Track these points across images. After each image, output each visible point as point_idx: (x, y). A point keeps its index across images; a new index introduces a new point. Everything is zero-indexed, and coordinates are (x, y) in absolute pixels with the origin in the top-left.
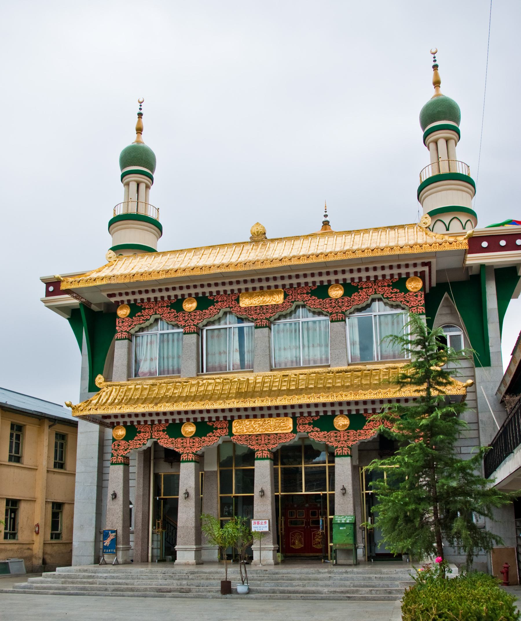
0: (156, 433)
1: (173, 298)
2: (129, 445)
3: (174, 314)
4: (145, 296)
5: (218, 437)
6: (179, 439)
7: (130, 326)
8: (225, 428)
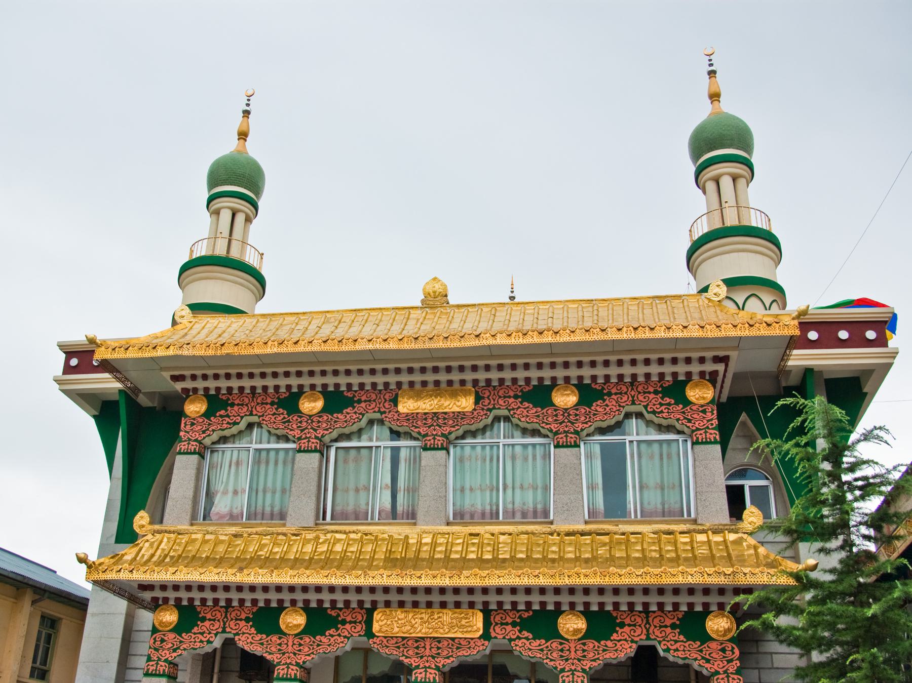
2: (181, 642)
4: (235, 384)
5: (345, 637)
6: (275, 638)
7: (204, 432)
8: (360, 622)
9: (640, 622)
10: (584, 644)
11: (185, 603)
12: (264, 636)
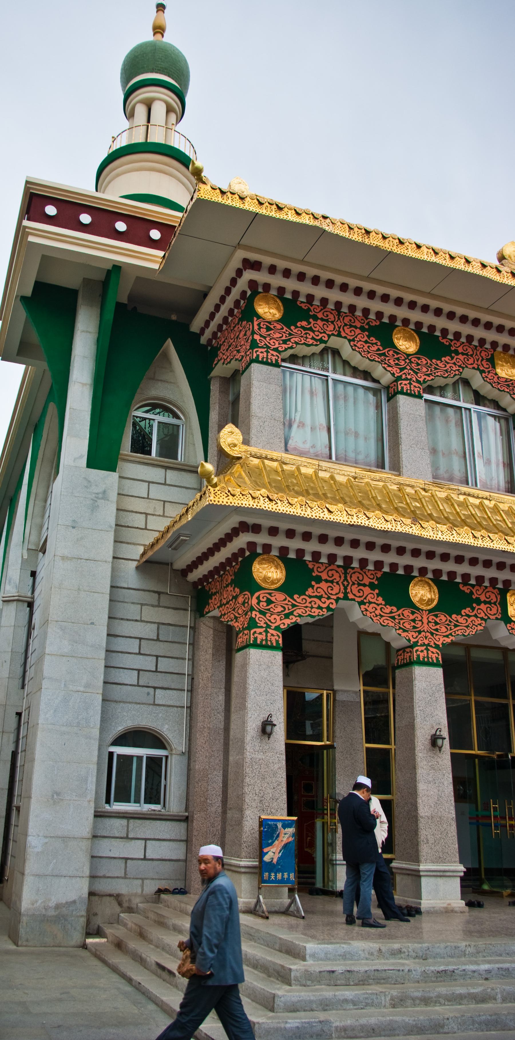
0: (355, 589)
1: (372, 316)
2: (294, 606)
3: (376, 348)
4: (320, 292)
5: (482, 619)
6: (407, 612)
7: (285, 342)
8: (495, 603)
9: (338, 579)
10: (436, 616)
11: (292, 555)
12: (395, 609)
